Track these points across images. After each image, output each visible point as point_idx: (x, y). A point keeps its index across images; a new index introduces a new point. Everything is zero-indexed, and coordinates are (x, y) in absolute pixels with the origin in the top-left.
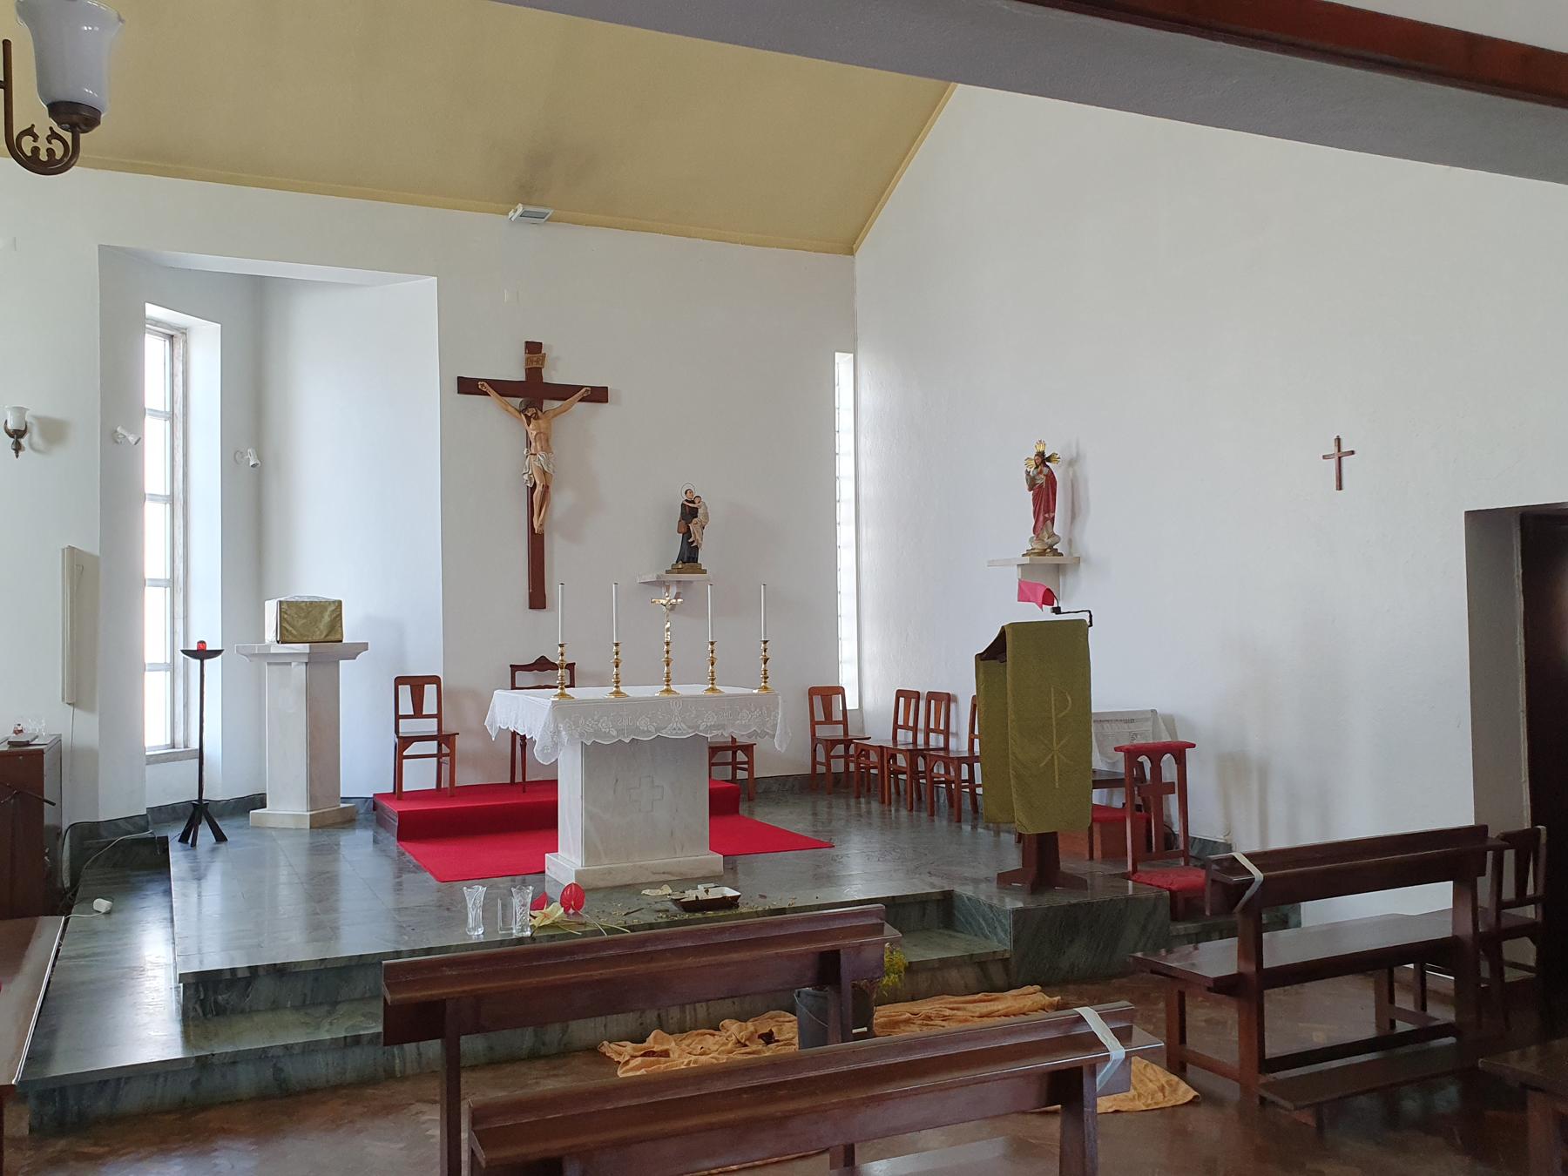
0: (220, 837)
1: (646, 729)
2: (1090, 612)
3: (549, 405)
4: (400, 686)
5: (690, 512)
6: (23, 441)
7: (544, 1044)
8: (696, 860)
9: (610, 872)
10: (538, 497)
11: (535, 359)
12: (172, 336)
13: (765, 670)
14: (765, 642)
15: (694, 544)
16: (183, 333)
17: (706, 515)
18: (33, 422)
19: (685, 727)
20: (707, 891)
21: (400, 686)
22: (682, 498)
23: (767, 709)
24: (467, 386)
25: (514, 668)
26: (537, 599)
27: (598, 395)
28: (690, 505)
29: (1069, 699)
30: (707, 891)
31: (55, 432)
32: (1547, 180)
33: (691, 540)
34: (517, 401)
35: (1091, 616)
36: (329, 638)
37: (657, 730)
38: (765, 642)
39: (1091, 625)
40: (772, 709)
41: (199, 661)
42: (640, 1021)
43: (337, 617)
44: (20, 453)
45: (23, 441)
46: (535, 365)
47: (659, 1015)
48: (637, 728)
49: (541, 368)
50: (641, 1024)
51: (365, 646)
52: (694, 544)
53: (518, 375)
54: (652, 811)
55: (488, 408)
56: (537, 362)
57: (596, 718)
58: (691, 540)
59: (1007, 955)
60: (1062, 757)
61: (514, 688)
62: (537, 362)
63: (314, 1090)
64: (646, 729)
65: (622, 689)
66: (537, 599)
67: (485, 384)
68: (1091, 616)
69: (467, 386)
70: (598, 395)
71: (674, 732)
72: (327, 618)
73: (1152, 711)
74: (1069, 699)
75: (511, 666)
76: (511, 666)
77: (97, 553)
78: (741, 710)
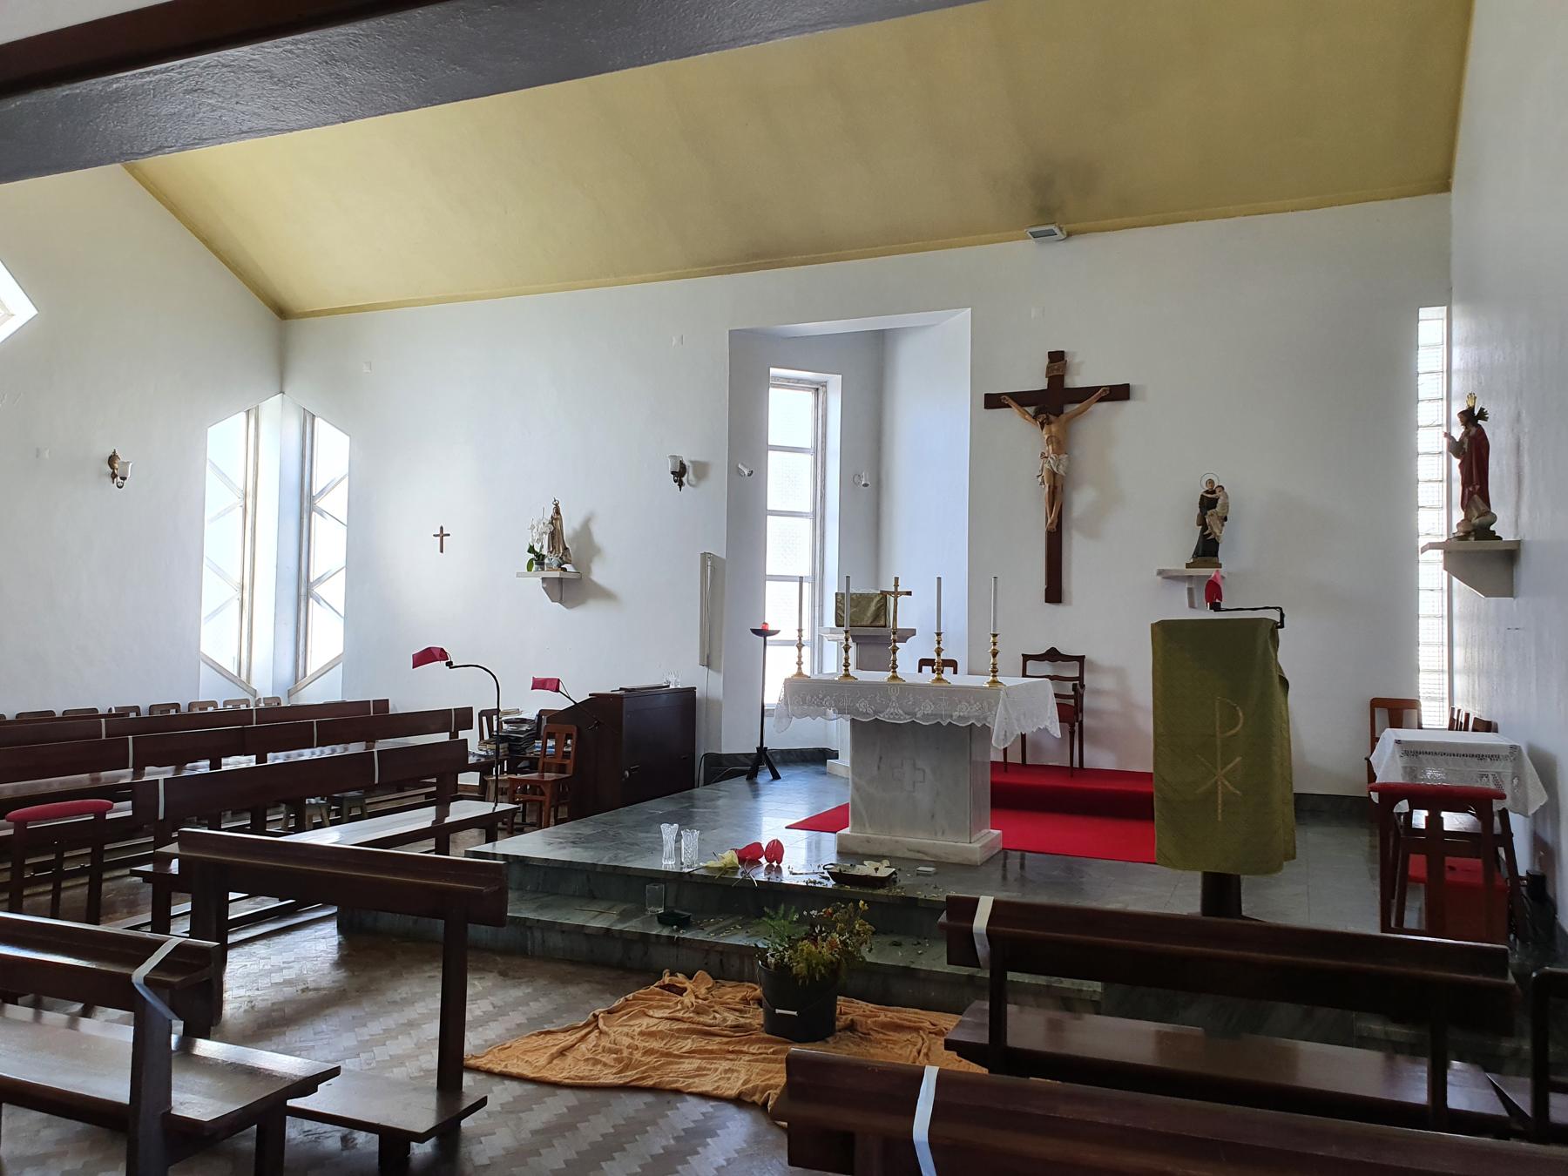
0: (776, 777)
1: (865, 711)
2: (1281, 609)
3: (1071, 409)
4: (923, 667)
5: (1209, 502)
6: (684, 479)
7: (630, 959)
8: (954, 846)
9: (868, 841)
10: (1057, 492)
11: (1056, 367)
12: (817, 389)
13: (994, 664)
14: (995, 636)
15: (1210, 537)
16: (823, 386)
17: (1226, 506)
18: (690, 464)
19: (901, 712)
20: (877, 869)
21: (923, 667)
22: (1201, 489)
23: (989, 703)
24: (993, 401)
25: (1026, 658)
26: (1054, 593)
27: (1120, 393)
28: (1209, 496)
29: (1241, 714)
30: (877, 869)
31: (702, 470)
32: (18, 180)
33: (1207, 532)
34: (1031, 410)
35: (1282, 615)
36: (873, 624)
37: (875, 712)
38: (995, 636)
39: (1282, 626)
40: (993, 704)
41: (762, 638)
42: (706, 961)
43: (881, 606)
44: (683, 488)
45: (684, 479)
46: (1055, 373)
47: (721, 960)
48: (857, 709)
49: (1063, 376)
50: (706, 964)
51: (913, 632)
52: (1210, 537)
53: (1040, 383)
54: (914, 792)
55: (1013, 420)
56: (1058, 370)
57: (821, 696)
58: (1207, 532)
59: (1096, 998)
60: (1226, 783)
61: (1024, 675)
62: (1058, 370)
63: (572, 962)
64: (865, 711)
65: (999, 679)
66: (1054, 593)
67: (1007, 397)
68: (1282, 615)
69: (993, 401)
70: (1120, 393)
71: (892, 717)
72: (873, 607)
73: (1512, 747)
74: (1241, 714)
75: (1023, 655)
76: (1023, 655)
77: (724, 557)
78: (960, 702)
